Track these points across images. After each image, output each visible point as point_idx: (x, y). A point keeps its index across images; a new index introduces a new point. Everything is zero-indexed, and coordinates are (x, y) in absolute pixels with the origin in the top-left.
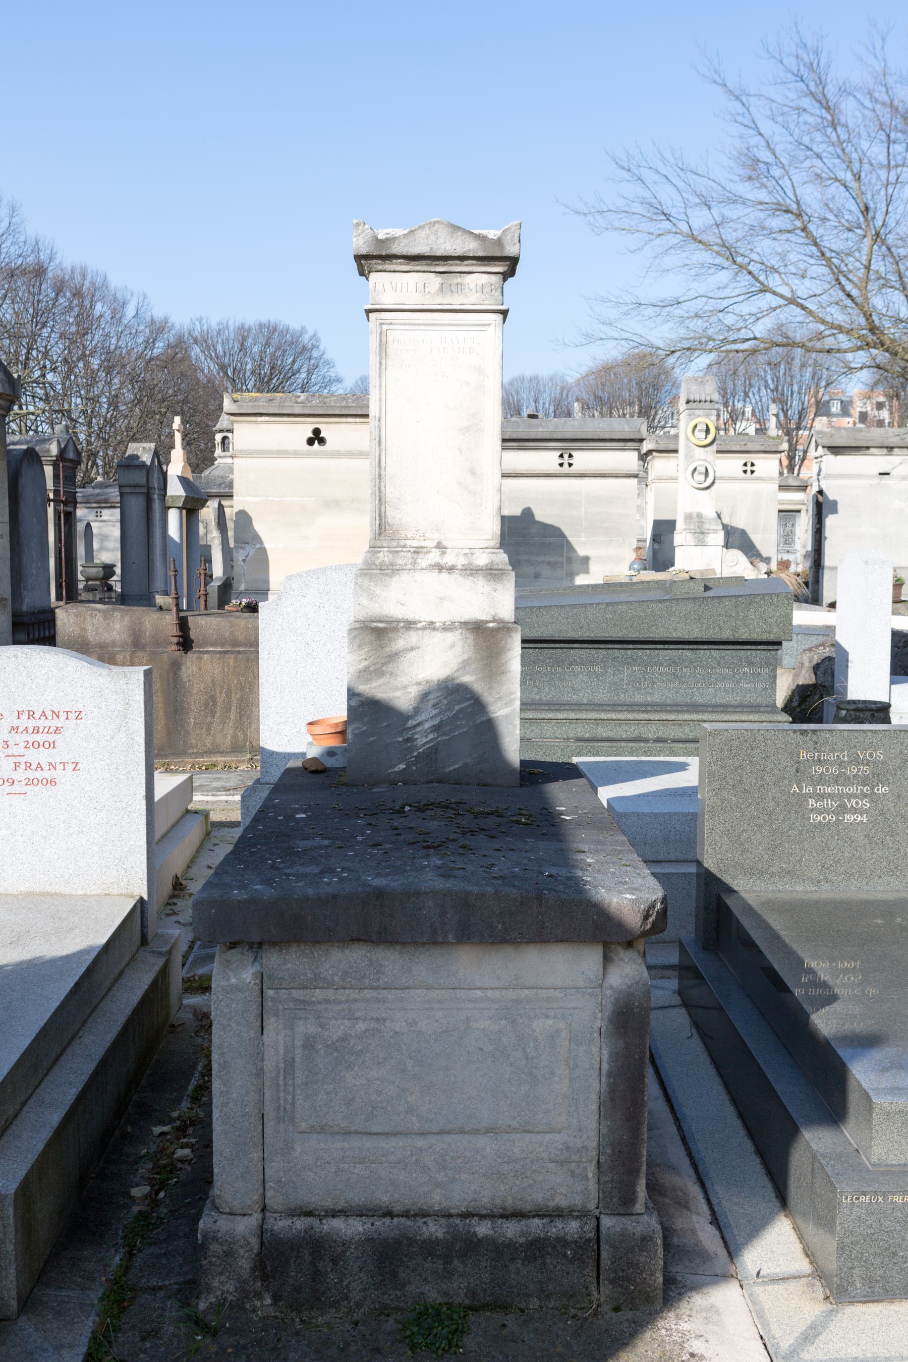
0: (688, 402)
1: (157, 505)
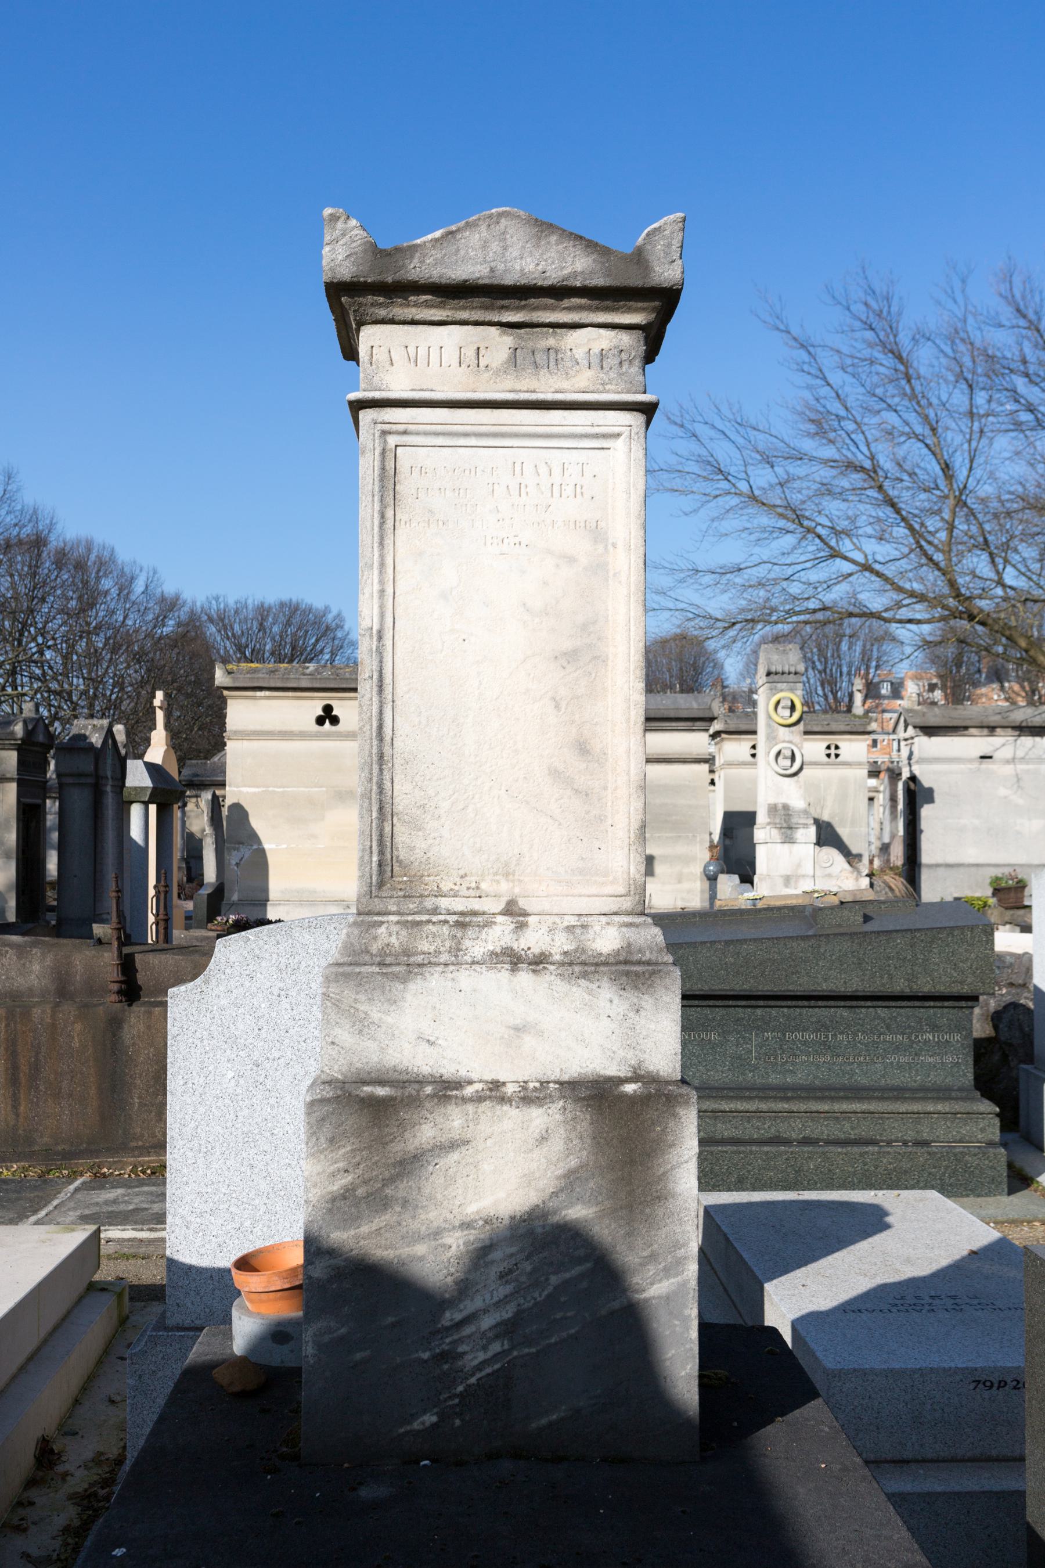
0: (769, 674)
1: (110, 800)
